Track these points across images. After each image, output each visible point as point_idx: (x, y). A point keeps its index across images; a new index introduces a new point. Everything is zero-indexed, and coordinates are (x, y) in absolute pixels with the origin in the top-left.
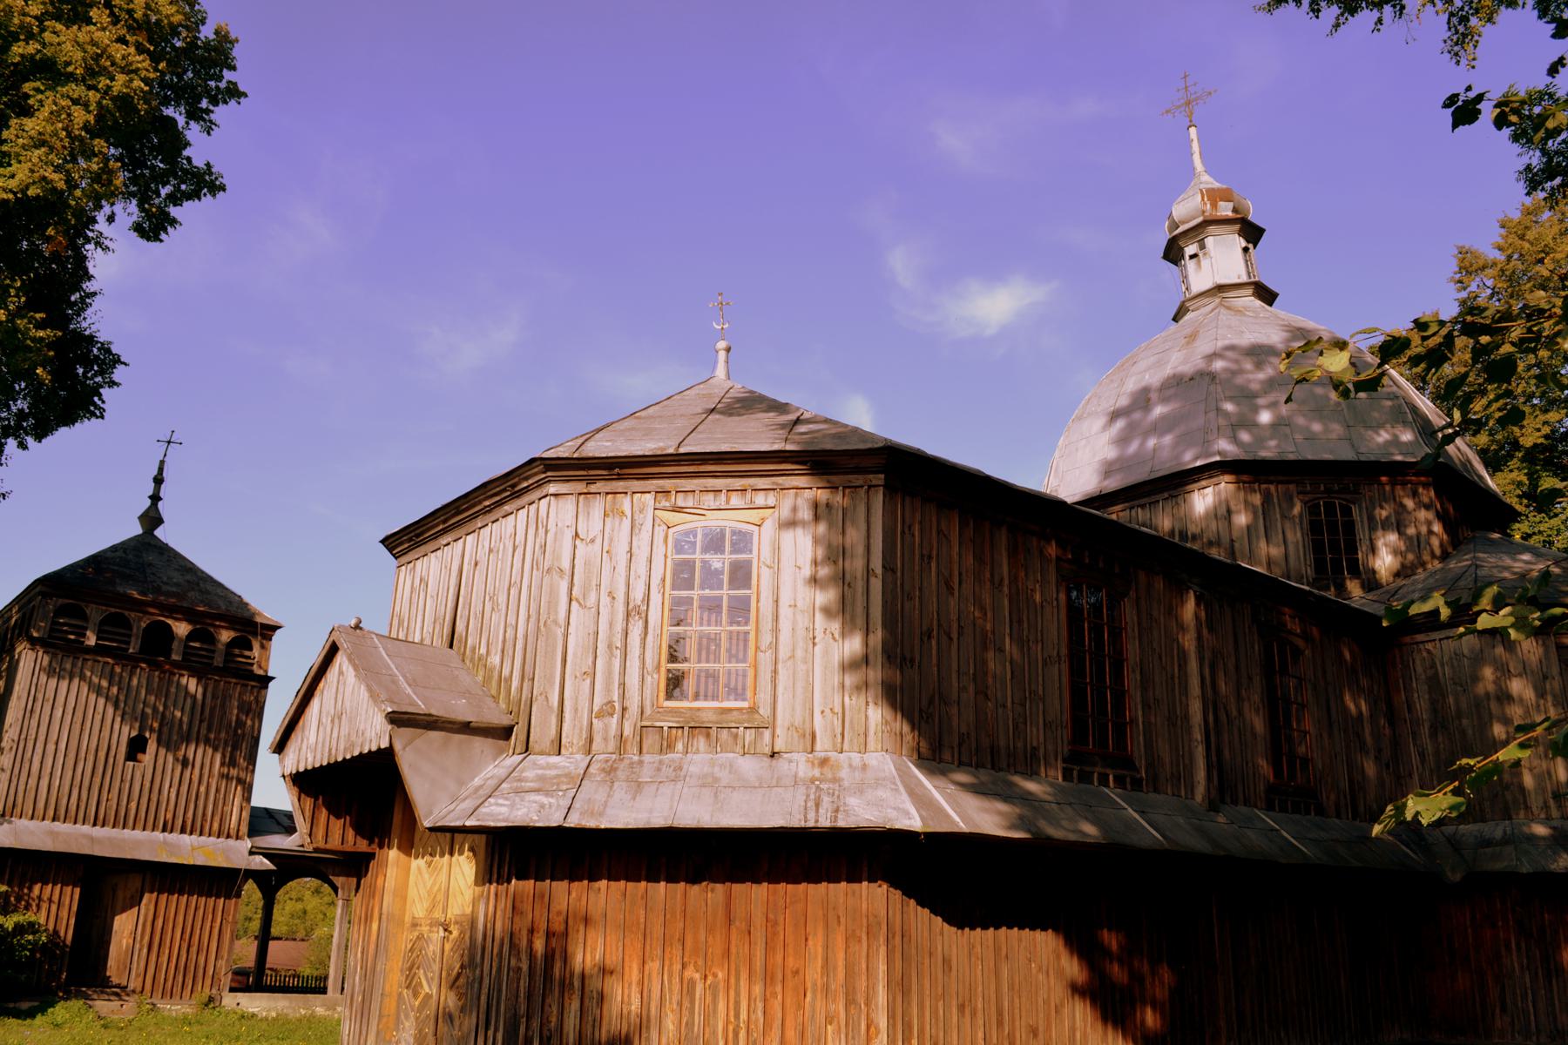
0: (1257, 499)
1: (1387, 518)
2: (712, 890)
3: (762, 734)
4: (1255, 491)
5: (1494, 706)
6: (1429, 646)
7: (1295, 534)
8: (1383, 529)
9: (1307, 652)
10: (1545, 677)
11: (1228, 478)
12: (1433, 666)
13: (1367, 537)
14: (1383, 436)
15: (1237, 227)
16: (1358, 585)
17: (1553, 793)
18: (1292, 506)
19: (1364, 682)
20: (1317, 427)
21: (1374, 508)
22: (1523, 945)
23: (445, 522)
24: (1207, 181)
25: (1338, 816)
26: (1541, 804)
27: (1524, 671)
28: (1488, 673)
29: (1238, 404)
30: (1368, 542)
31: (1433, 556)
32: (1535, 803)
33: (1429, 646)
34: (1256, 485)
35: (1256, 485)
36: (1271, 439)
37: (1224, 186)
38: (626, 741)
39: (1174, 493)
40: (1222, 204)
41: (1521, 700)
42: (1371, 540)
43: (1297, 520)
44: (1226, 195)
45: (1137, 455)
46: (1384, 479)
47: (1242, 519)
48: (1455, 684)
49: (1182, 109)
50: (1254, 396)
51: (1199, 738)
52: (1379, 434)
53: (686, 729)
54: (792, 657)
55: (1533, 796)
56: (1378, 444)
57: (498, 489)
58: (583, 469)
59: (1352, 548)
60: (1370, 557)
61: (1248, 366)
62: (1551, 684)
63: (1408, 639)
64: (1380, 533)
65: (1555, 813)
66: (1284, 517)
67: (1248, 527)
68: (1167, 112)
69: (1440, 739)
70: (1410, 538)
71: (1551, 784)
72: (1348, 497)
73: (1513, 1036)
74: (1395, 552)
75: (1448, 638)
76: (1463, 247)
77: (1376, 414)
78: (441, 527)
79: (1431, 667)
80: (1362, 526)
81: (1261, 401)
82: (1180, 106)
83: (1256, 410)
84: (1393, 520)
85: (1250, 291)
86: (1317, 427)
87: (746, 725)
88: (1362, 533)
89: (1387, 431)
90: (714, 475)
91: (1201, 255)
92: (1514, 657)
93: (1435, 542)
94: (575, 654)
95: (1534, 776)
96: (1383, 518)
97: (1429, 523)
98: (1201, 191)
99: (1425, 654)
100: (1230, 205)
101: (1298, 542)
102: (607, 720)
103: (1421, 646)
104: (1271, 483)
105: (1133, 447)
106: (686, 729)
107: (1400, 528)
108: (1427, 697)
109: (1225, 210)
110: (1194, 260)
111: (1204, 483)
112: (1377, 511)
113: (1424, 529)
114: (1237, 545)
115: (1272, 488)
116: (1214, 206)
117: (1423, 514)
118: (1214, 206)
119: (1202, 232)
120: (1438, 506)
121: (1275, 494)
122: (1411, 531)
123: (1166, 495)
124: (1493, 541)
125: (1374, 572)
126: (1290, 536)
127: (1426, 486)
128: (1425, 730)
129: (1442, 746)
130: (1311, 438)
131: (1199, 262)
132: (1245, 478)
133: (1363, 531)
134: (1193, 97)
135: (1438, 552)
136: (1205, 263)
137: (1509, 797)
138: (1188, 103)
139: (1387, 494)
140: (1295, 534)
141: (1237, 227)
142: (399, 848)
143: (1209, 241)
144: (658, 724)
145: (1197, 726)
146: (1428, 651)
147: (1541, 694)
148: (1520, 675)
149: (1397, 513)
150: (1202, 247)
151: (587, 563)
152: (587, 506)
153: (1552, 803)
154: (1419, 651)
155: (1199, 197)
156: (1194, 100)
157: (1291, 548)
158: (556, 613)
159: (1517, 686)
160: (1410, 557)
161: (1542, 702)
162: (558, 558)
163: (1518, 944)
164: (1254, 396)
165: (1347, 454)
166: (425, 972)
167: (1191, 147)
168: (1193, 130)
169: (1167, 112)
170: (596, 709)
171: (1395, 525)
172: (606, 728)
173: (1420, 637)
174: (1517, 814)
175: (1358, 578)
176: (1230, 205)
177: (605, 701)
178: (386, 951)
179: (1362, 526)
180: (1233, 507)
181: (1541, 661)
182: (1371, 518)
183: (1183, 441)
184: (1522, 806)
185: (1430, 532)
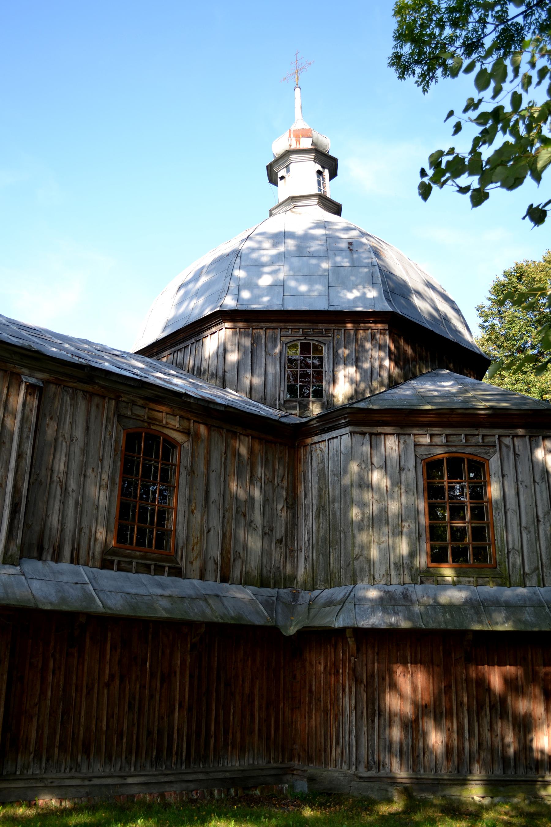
0: (247, 342)
1: (349, 355)
4: (248, 335)
5: (355, 492)
6: (322, 445)
7: (275, 367)
8: (345, 364)
9: (186, 445)
10: (401, 469)
11: (227, 325)
12: (322, 462)
13: (331, 370)
14: (352, 295)
16: (319, 406)
17: (395, 564)
18: (275, 347)
19: (260, 471)
20: (303, 288)
21: (340, 348)
22: (353, 689)
24: (300, 124)
25: (202, 577)
26: (383, 572)
27: (385, 466)
28: (354, 467)
29: (247, 271)
30: (331, 374)
31: (381, 384)
32: (379, 572)
34: (250, 330)
35: (250, 330)
36: (266, 296)
39: (197, 338)
41: (379, 488)
42: (333, 371)
43: (278, 357)
44: (307, 134)
45: (183, 313)
46: (349, 326)
47: (233, 357)
48: (334, 475)
50: (263, 265)
52: (351, 292)
55: (377, 566)
56: (349, 300)
59: (319, 376)
60: (332, 386)
62: (406, 474)
63: (309, 441)
64: (341, 367)
65: (394, 580)
66: (266, 353)
67: (238, 362)
69: (321, 520)
70: (365, 371)
71: (395, 555)
72: (321, 339)
73: (341, 766)
74: (352, 381)
75: (333, 438)
77: (353, 278)
79: (321, 462)
80: (329, 362)
81: (267, 269)
83: (260, 275)
84: (354, 357)
86: (303, 288)
88: (327, 367)
89: (358, 290)
92: (378, 454)
93: (385, 374)
95: (380, 550)
96: (345, 355)
97: (381, 359)
98: (290, 130)
99: (319, 452)
101: (276, 372)
104: (262, 329)
105: (181, 310)
107: (357, 363)
108: (316, 486)
109: (306, 144)
111: (214, 329)
112: (341, 351)
113: (377, 364)
114: (228, 375)
115: (262, 332)
116: (298, 141)
117: (376, 354)
118: (298, 141)
119: (287, 160)
120: (392, 347)
121: (263, 337)
122: (366, 365)
123: (193, 340)
124: (443, 375)
125: (333, 396)
126: (270, 370)
127: (382, 332)
128: (312, 514)
129: (321, 525)
130: (298, 295)
132: (241, 324)
133: (329, 365)
134: (300, 67)
135: (386, 381)
137: (357, 565)
139: (352, 336)
140: (275, 367)
141: (312, 156)
145: (8, 494)
146: (321, 450)
147: (397, 483)
148: (380, 468)
149: (357, 352)
153: (393, 573)
156: (301, 69)
157: (270, 377)
159: (376, 477)
160: (362, 386)
161: (396, 489)
163: (350, 688)
164: (263, 265)
165: (321, 305)
167: (294, 102)
168: (298, 90)
171: (354, 360)
173: (316, 439)
174: (362, 580)
175: (320, 401)
176: (310, 141)
178: (482, 725)
179: (329, 362)
180: (229, 347)
181: (400, 456)
182: (336, 356)
183: (207, 302)
184: (367, 574)
185: (381, 366)
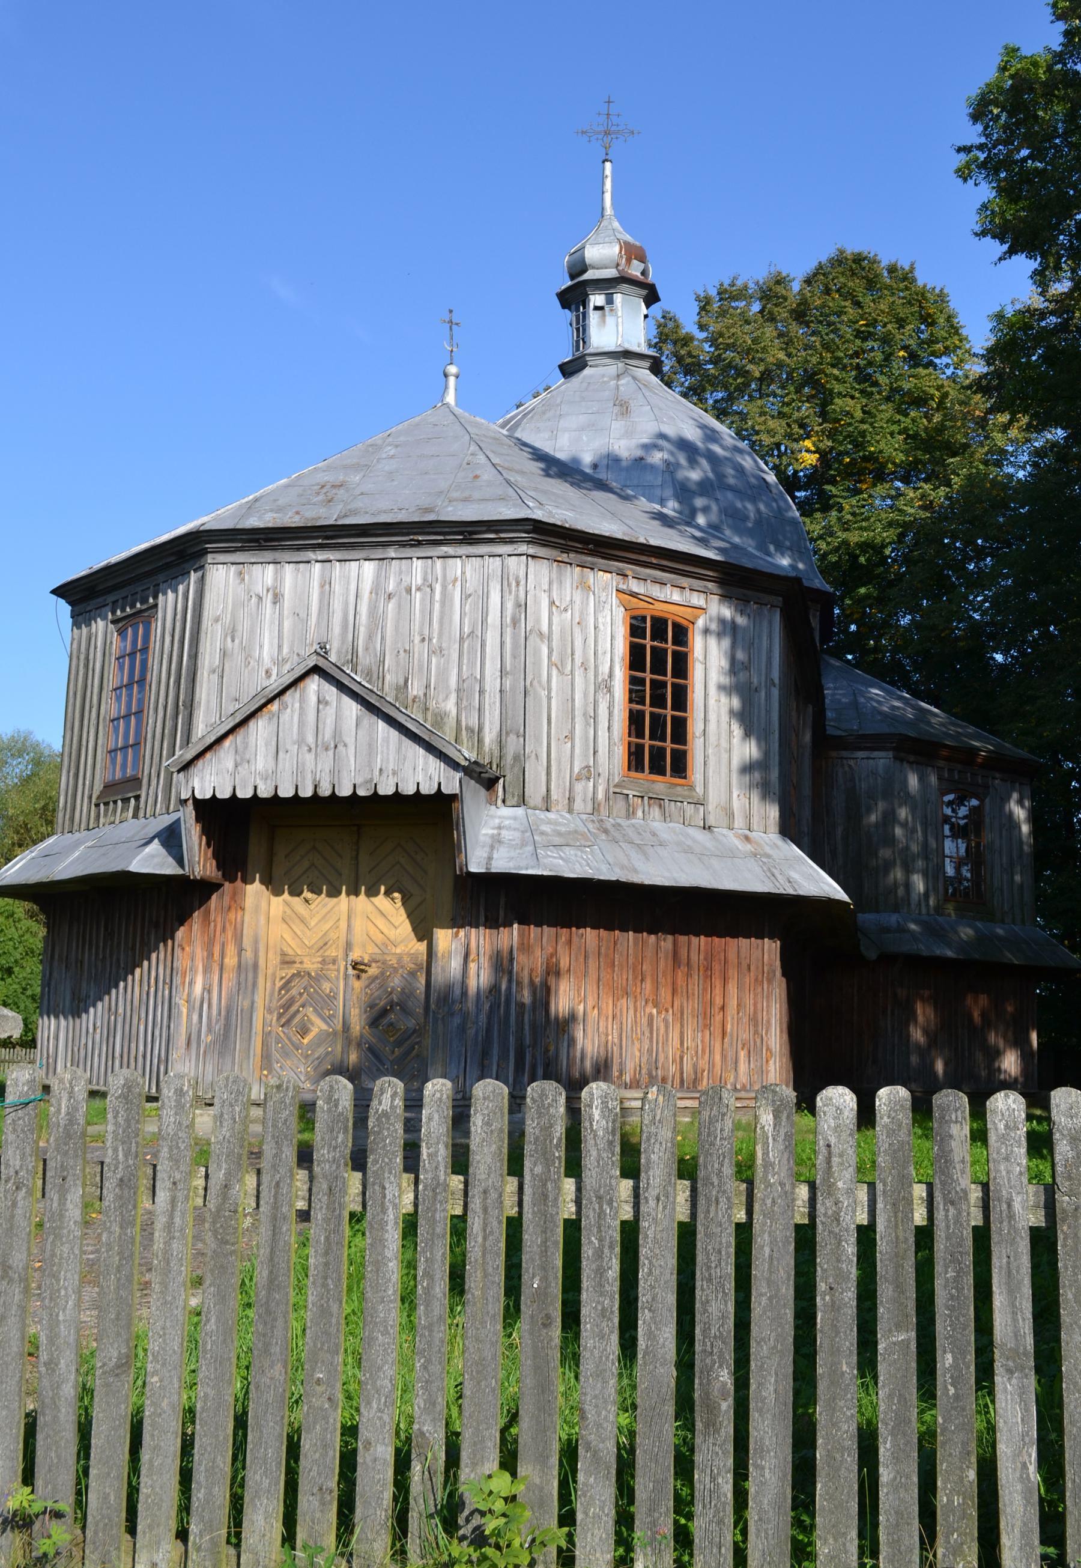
2: (665, 940)
3: (698, 809)
6: (852, 762)
15: (644, 292)
23: (327, 538)
33: (852, 762)
37: (638, 243)
38: (599, 805)
40: (635, 262)
49: (600, 137)
51: (806, 830)
53: (646, 798)
54: (718, 746)
57: (447, 530)
58: (564, 538)
61: (683, 460)
63: (834, 754)
68: (583, 132)
76: (669, 313)
78: (320, 541)
82: (599, 133)
85: (647, 364)
87: (651, 795)
90: (663, 569)
91: (607, 309)
94: (557, 717)
99: (847, 768)
100: (642, 266)
102: (583, 782)
103: (845, 761)
106: (646, 798)
110: (598, 313)
116: (629, 261)
118: (629, 261)
119: (615, 287)
131: (604, 316)
136: (610, 320)
138: (607, 133)
141: (644, 292)
142: (262, 882)
143: (618, 298)
144: (625, 792)
146: (850, 766)
150: (610, 301)
151: (562, 631)
152: (560, 574)
154: (843, 765)
155: (617, 249)
158: (540, 676)
162: (538, 621)
166: (315, 1010)
167: (603, 184)
168: (608, 165)
169: (583, 132)
170: (576, 770)
172: (585, 788)
173: (845, 754)
177: (583, 765)
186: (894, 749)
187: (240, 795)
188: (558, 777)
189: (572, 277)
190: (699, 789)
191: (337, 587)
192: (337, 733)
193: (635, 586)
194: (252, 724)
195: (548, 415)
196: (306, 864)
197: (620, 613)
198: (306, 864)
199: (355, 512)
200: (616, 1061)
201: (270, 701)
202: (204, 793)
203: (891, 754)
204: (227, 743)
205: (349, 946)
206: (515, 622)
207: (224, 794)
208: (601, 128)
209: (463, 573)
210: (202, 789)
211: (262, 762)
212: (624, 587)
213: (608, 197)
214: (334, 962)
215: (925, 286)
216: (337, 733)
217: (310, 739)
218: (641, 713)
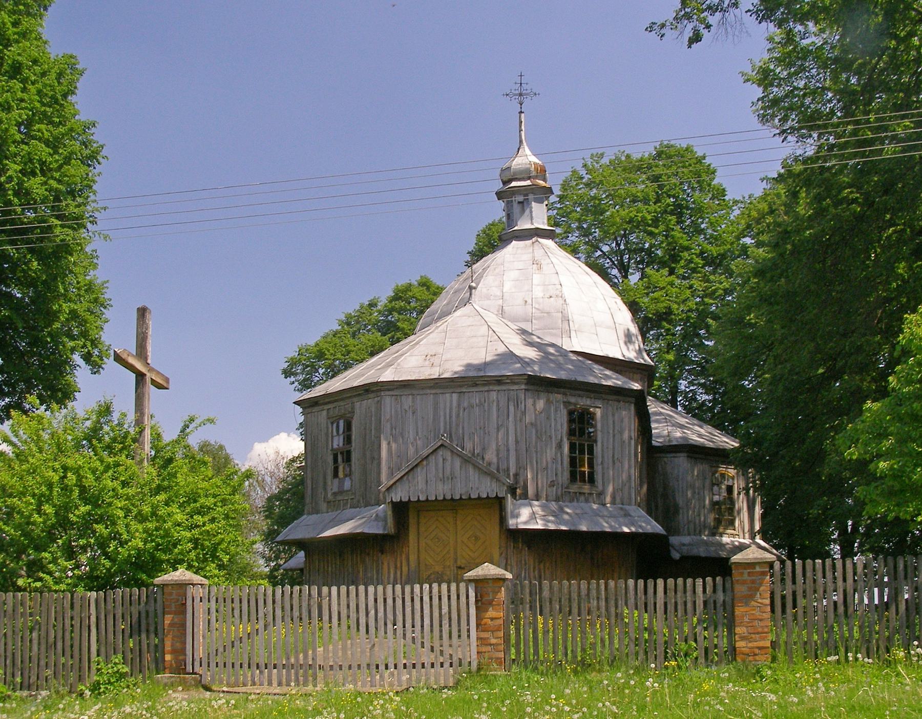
131: (523, 206)
138: (521, 95)
168: (523, 115)
169: (507, 95)
173: (664, 455)
186: (687, 452)
187: (403, 500)
188: (367, 368)
189: (505, 183)
190: (600, 488)
191: (442, 405)
192: (452, 473)
193: (573, 400)
194: (415, 470)
195: (497, 271)
196: (434, 527)
197: (565, 412)
198: (434, 527)
199: (445, 371)
200: (623, 345)
201: (423, 460)
202: (396, 499)
203: (686, 455)
204: (405, 478)
205: (456, 561)
206: (521, 421)
207: (405, 499)
208: (517, 92)
209: (497, 398)
210: (405, 497)
211: (421, 485)
212: (565, 400)
213: (523, 133)
214: (449, 567)
215: (709, 165)
216: (452, 473)
217: (441, 475)
218: (575, 444)
